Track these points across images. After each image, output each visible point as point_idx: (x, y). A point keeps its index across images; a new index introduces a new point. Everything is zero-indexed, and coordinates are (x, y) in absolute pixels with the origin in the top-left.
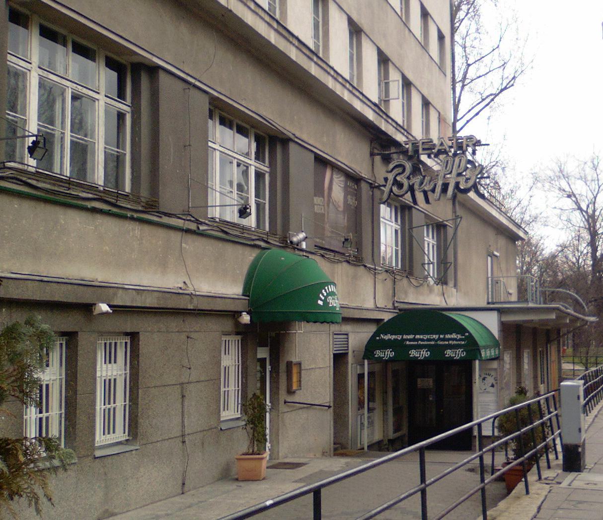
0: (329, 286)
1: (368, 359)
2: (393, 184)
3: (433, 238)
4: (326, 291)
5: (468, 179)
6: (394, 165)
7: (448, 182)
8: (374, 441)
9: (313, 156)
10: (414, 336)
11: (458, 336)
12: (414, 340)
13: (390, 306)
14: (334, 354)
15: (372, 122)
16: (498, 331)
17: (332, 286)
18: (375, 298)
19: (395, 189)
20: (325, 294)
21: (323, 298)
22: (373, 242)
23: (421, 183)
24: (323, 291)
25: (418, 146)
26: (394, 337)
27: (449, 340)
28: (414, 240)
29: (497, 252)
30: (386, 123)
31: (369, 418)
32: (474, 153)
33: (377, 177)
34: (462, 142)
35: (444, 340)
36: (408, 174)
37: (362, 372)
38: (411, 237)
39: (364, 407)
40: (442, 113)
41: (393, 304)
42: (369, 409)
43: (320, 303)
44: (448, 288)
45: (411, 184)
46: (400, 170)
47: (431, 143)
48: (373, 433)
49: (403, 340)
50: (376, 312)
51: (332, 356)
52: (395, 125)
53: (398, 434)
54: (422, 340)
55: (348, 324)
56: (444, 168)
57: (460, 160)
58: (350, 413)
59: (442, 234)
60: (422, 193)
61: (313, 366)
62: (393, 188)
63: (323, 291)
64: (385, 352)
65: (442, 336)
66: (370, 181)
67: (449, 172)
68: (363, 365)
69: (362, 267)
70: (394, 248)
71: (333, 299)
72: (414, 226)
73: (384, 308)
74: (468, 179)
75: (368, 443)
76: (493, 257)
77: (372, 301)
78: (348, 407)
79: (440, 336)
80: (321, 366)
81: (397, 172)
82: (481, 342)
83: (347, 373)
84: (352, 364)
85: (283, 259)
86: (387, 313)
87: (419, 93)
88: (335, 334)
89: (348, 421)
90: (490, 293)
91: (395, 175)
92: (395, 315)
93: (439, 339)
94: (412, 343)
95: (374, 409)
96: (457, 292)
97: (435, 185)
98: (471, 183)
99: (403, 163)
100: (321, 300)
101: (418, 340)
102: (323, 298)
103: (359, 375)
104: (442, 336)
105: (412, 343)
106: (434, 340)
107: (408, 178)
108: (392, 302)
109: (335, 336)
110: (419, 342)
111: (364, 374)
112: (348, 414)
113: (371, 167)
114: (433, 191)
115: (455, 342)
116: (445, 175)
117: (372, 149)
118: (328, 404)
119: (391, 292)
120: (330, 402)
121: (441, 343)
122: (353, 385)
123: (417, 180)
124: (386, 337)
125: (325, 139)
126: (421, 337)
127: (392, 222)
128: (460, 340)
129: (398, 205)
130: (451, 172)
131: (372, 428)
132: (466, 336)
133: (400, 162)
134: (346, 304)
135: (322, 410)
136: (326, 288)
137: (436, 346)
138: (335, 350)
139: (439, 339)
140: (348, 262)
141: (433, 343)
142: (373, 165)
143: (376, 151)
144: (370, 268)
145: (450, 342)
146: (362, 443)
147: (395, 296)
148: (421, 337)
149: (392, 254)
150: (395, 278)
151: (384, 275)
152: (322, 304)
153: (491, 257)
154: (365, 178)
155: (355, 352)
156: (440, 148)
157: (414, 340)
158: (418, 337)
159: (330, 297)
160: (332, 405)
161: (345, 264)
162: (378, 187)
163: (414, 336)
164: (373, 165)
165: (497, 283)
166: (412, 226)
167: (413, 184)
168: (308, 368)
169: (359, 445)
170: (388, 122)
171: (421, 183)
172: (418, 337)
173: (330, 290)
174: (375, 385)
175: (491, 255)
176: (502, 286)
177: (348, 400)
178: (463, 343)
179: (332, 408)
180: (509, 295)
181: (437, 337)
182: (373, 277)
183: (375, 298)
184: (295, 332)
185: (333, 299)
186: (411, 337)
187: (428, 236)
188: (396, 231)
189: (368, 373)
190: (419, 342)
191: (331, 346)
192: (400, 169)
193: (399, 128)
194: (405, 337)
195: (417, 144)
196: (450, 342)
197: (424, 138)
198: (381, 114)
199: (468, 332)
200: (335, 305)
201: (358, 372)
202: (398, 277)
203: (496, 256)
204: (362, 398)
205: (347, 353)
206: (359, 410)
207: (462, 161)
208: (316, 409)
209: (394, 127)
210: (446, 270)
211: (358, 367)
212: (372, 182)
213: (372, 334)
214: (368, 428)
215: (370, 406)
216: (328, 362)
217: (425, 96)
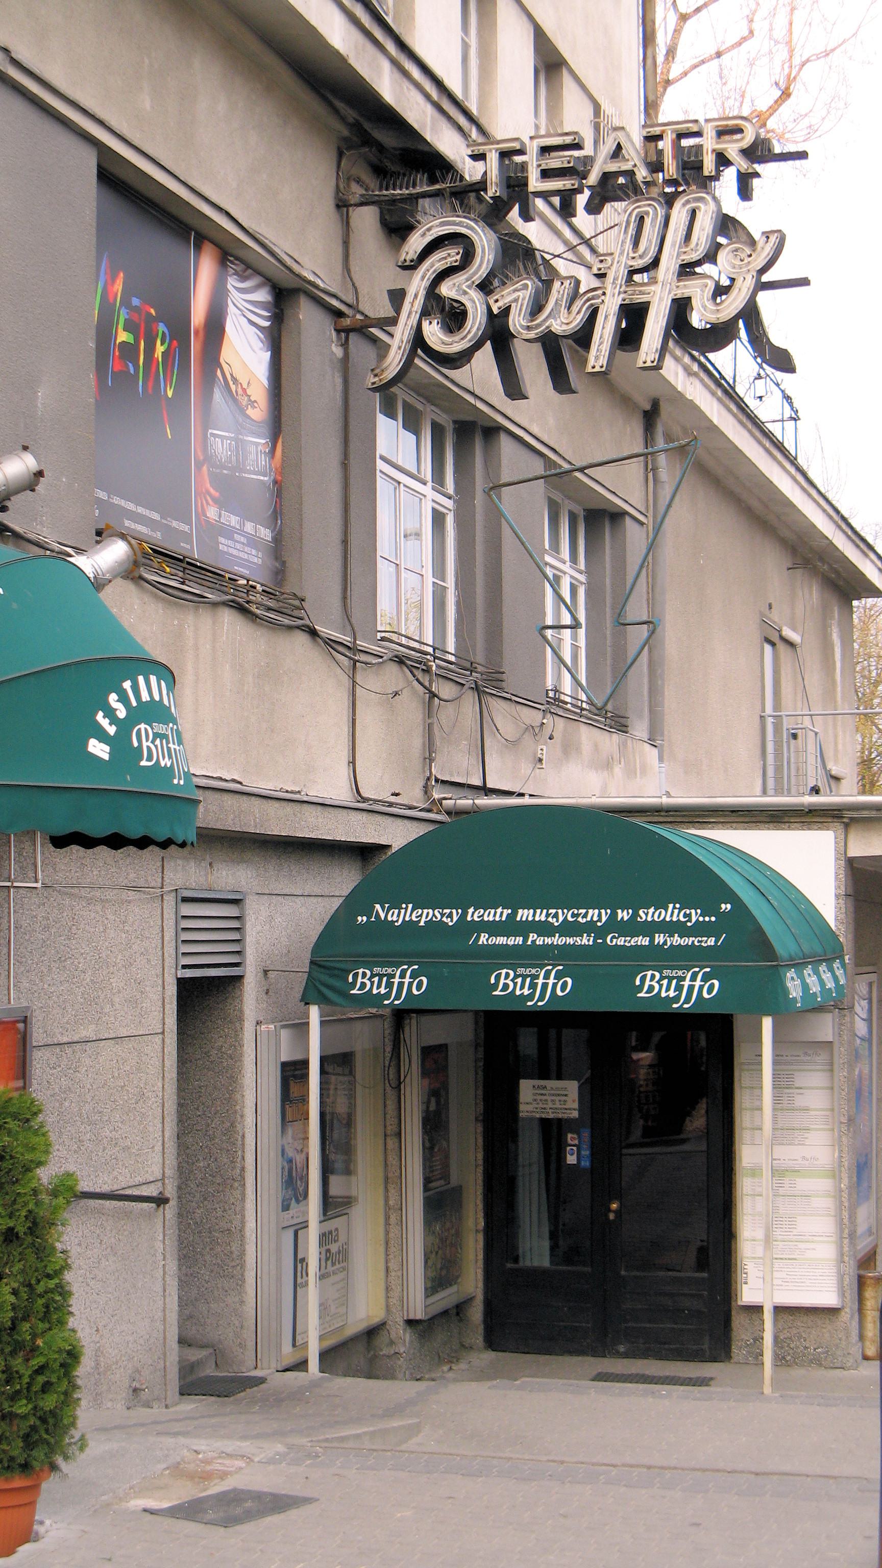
0: (141, 679)
1: (323, 1000)
2: (425, 313)
3: (574, 558)
4: (123, 699)
5: (720, 291)
6: (429, 238)
7: (643, 298)
8: (350, 1331)
9: (89, 161)
10: (507, 912)
11: (688, 916)
12: (510, 927)
13: (413, 795)
14: (181, 982)
15: (343, 59)
16: (837, 896)
17: (153, 679)
18: (353, 762)
19: (433, 332)
20: (122, 713)
21: (112, 730)
22: (345, 542)
23: (537, 308)
24: (113, 698)
25: (523, 167)
26: (424, 916)
27: (650, 929)
28: (506, 532)
29: (794, 629)
30: (397, 75)
31: (325, 1238)
32: (745, 192)
33: (363, 290)
34: (699, 148)
35: (633, 928)
36: (483, 272)
37: (298, 1057)
38: (495, 516)
39: (306, 1195)
40: (605, 106)
41: (426, 789)
42: (327, 1202)
43: (98, 749)
44: (629, 742)
45: (495, 311)
46: (450, 256)
47: (576, 153)
48: (345, 1297)
49: (467, 928)
50: (354, 816)
51: (172, 990)
52: (434, 93)
53: (446, 1298)
54: (545, 929)
55: (242, 861)
56: (628, 245)
57: (693, 213)
58: (250, 1225)
59: (608, 558)
60: (537, 348)
61: (88, 1032)
62: (425, 325)
63: (113, 698)
64: (536, 977)
65: (623, 915)
66: (335, 303)
67: (648, 259)
68: (302, 1027)
69: (302, 638)
70: (430, 579)
71: (156, 735)
72: (505, 479)
73: (391, 805)
74: (720, 291)
75: (321, 1338)
76: (781, 647)
77: (344, 771)
78: (243, 1195)
79: (614, 915)
80: (124, 1032)
81: (440, 266)
82: (784, 945)
83: (236, 1057)
84: (258, 1023)
85: (15, 606)
86: (399, 822)
87: (525, 18)
88: (185, 900)
89: (242, 1253)
90: (770, 772)
91: (430, 275)
92: (431, 827)
93: (613, 926)
94: (501, 940)
95: (348, 1202)
96: (661, 759)
97: (594, 313)
98: (733, 304)
99: (463, 231)
100: (103, 736)
101: (525, 928)
102: (112, 730)
103: (284, 1065)
104: (623, 915)
105: (501, 940)
106: (590, 928)
107: (485, 287)
108: (422, 783)
109: (188, 909)
110: (532, 937)
111: (305, 1063)
112: (243, 1222)
113: (339, 250)
114: (583, 337)
115: (677, 940)
116: (632, 272)
117: (343, 179)
118: (151, 1191)
119: (417, 742)
120: (163, 1179)
121: (621, 941)
122: (264, 1107)
123: (520, 294)
124: (396, 917)
125: (146, 102)
126: (541, 916)
127: (425, 484)
128: (700, 930)
129: (444, 419)
130: (655, 263)
131: (342, 1275)
132: (721, 915)
133: (454, 223)
134: (234, 781)
135: (128, 1214)
136: (127, 685)
137: (600, 952)
138: (184, 967)
139: (613, 926)
140: (242, 610)
141: (585, 940)
142: (346, 243)
143: (357, 191)
144: (331, 643)
145: (659, 939)
146: (299, 1341)
147: (431, 760)
148: (541, 916)
149: (422, 595)
150: (433, 695)
151: (393, 677)
152: (106, 757)
153: (773, 644)
154: (317, 287)
155: (271, 975)
156: (613, 167)
157: (510, 927)
158: (524, 914)
159: (143, 726)
160: (170, 1191)
161: (228, 617)
162: (362, 329)
163: (507, 912)
164: (346, 243)
165: (795, 736)
166: (498, 476)
167: (506, 311)
168: (65, 1039)
169: (287, 1348)
170: (406, 74)
171: (537, 308)
172: (524, 914)
173: (145, 697)
174: (352, 1106)
175: (776, 638)
176: (811, 748)
177: (243, 1169)
178: (711, 942)
179: (170, 1210)
180: (832, 782)
181: (604, 919)
182: (346, 681)
183: (353, 762)
184: (9, 884)
185: (156, 735)
186: (500, 914)
187: (555, 547)
188: (438, 519)
189: (323, 1060)
190: (532, 937)
191: (170, 950)
192: (453, 252)
193: (447, 105)
194: (473, 915)
195: (518, 159)
196: (659, 939)
197: (543, 132)
198: (378, 34)
199: (732, 897)
200: (165, 762)
201: (284, 1058)
202: (446, 690)
203: (791, 644)
204: (299, 1158)
205: (239, 978)
206: (286, 1208)
207: (699, 216)
208: (101, 1212)
209: (427, 97)
210: (621, 674)
211: (285, 1034)
212: (343, 308)
213: (337, 903)
214: (322, 1277)
215: (333, 1191)
216: (158, 1015)
217: (549, 34)
